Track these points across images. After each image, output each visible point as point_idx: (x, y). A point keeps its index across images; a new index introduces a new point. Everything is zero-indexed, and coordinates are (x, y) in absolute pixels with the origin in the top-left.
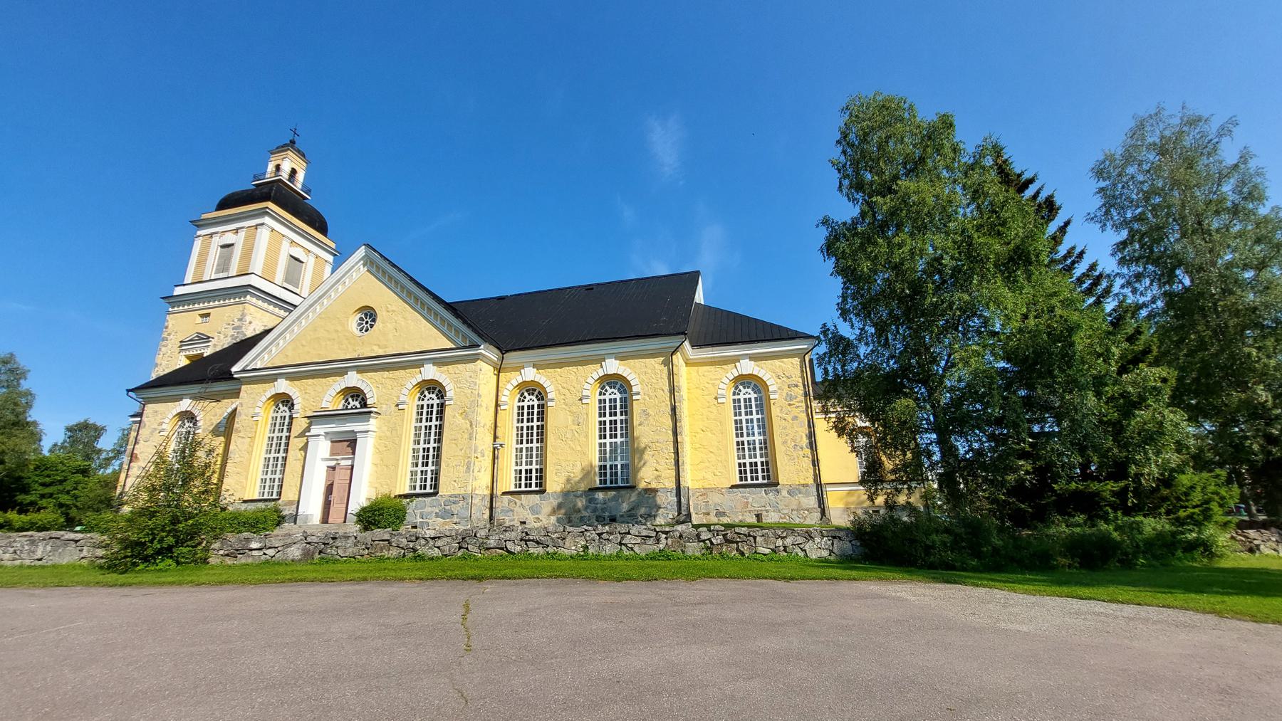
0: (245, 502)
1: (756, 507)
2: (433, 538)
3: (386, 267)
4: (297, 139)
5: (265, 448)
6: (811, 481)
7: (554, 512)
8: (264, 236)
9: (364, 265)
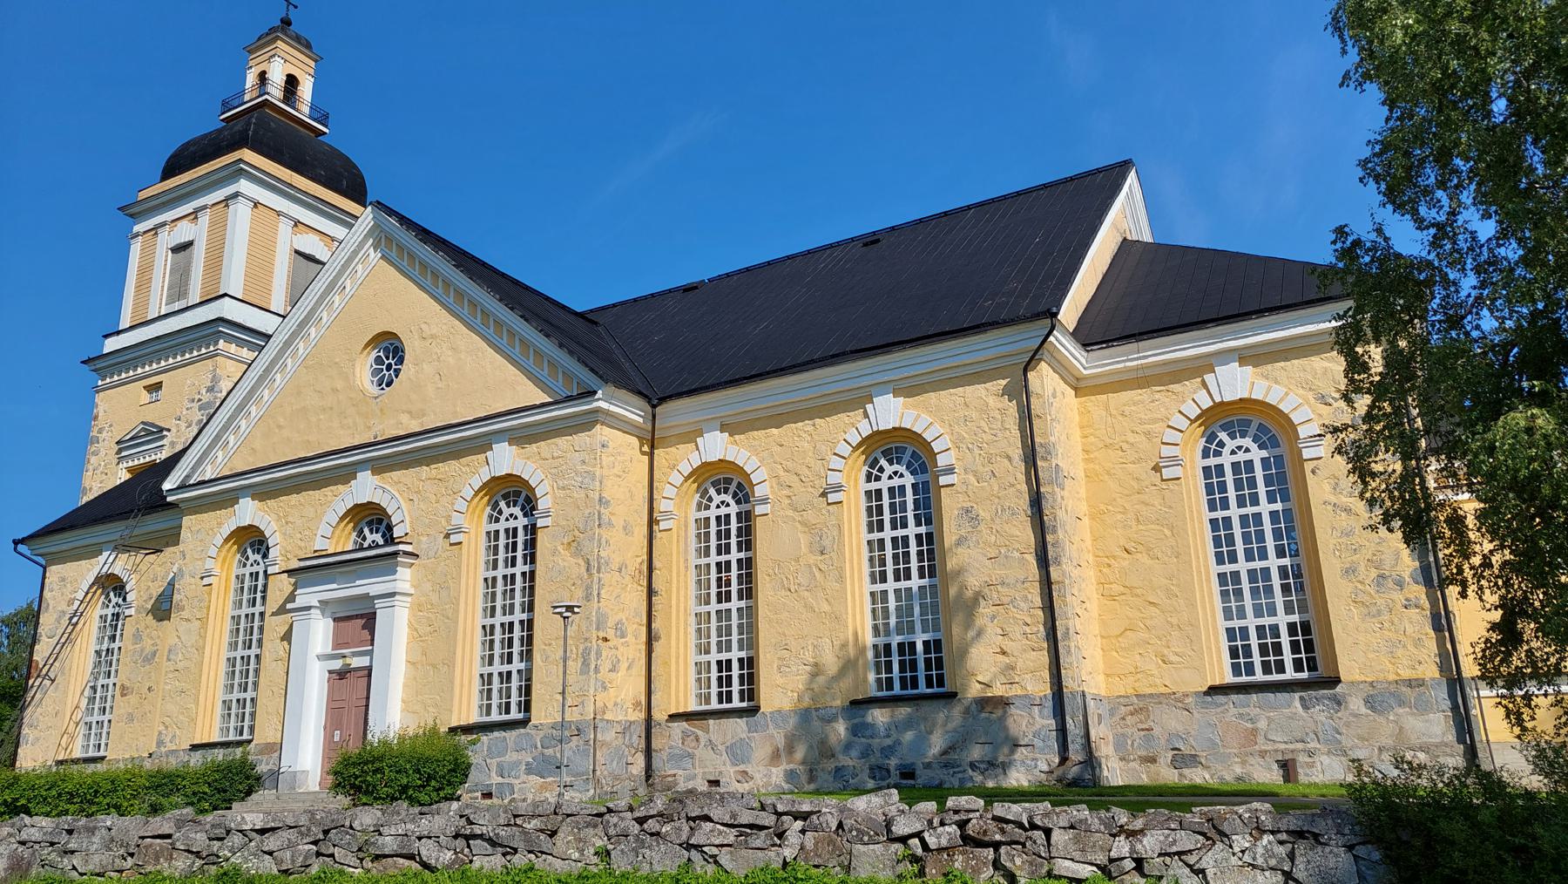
0: (195, 747)
1: (1281, 743)
2: (262, 832)
3: (440, 253)
4: (293, 15)
5: (226, 638)
6: (1431, 671)
7: (775, 757)
8: (241, 213)
9: (376, 247)
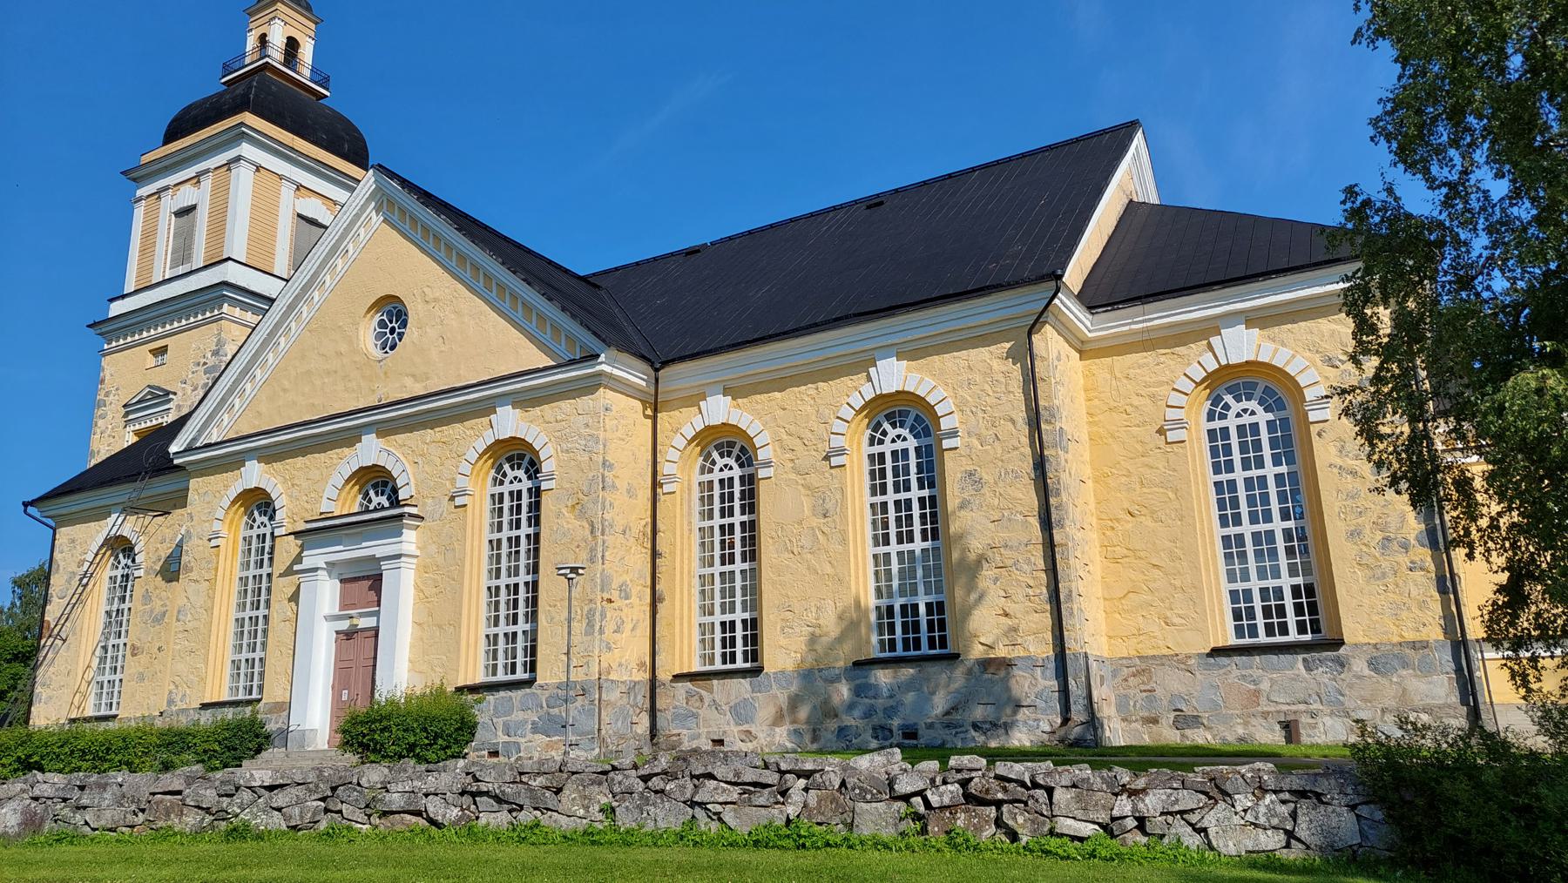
0: (205, 706)
1: (1283, 704)
2: (271, 788)
5: (234, 599)
6: (1435, 633)
7: (778, 720)
8: (243, 177)
